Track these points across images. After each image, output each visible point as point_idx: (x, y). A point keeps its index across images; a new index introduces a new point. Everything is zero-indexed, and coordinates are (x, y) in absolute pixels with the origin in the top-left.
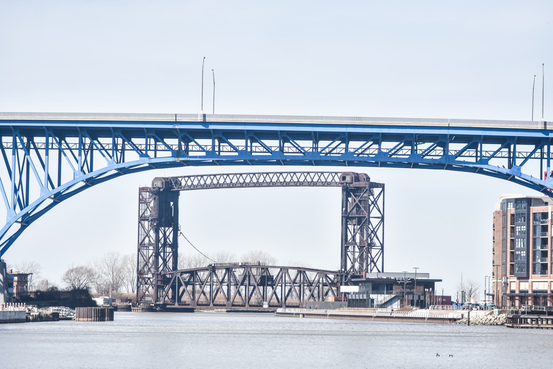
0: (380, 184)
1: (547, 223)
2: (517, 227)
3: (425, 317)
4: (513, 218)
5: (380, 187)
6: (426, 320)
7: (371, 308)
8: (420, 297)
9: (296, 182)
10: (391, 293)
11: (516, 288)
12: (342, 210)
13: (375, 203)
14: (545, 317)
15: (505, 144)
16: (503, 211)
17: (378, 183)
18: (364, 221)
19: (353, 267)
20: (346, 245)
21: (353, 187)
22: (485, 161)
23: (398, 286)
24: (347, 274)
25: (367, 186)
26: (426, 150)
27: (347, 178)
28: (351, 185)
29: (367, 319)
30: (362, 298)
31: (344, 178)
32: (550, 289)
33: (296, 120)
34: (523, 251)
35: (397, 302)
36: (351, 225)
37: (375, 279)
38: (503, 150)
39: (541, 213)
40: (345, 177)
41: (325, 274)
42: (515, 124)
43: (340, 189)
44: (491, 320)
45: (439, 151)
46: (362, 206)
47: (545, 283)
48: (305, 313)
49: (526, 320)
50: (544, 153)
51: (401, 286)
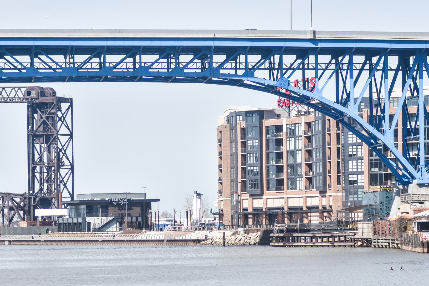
0: (68, 99)
1: (281, 137)
2: (249, 142)
3: (163, 239)
4: (243, 132)
5: (68, 102)
6: (165, 243)
7: (87, 232)
8: (138, 218)
9: (6, 98)
10: (107, 215)
11: (249, 205)
12: (28, 128)
13: (63, 119)
14: (320, 235)
15: (165, 54)
16: (230, 125)
17: (66, 97)
18: (52, 139)
19: (41, 189)
20: (33, 166)
21: (40, 103)
22: (249, 73)
23: (113, 208)
24: (36, 196)
25: (55, 101)
26: (257, 63)
27: (32, 93)
28: (37, 101)
29: (77, 243)
30: (76, 221)
31: (29, 93)
32: (287, 205)
33: (53, 34)
34: (256, 166)
35: (115, 225)
36: (38, 143)
37: (89, 200)
38: (161, 61)
39: (275, 126)
40: (30, 92)
41: (11, 198)
42: (282, 34)
43: (24, 106)
44: (241, 240)
45: (198, 63)
46: (50, 123)
47: (312, 198)
48: (12, 240)
49: (299, 238)
50: (171, 63)
51: (117, 208)
